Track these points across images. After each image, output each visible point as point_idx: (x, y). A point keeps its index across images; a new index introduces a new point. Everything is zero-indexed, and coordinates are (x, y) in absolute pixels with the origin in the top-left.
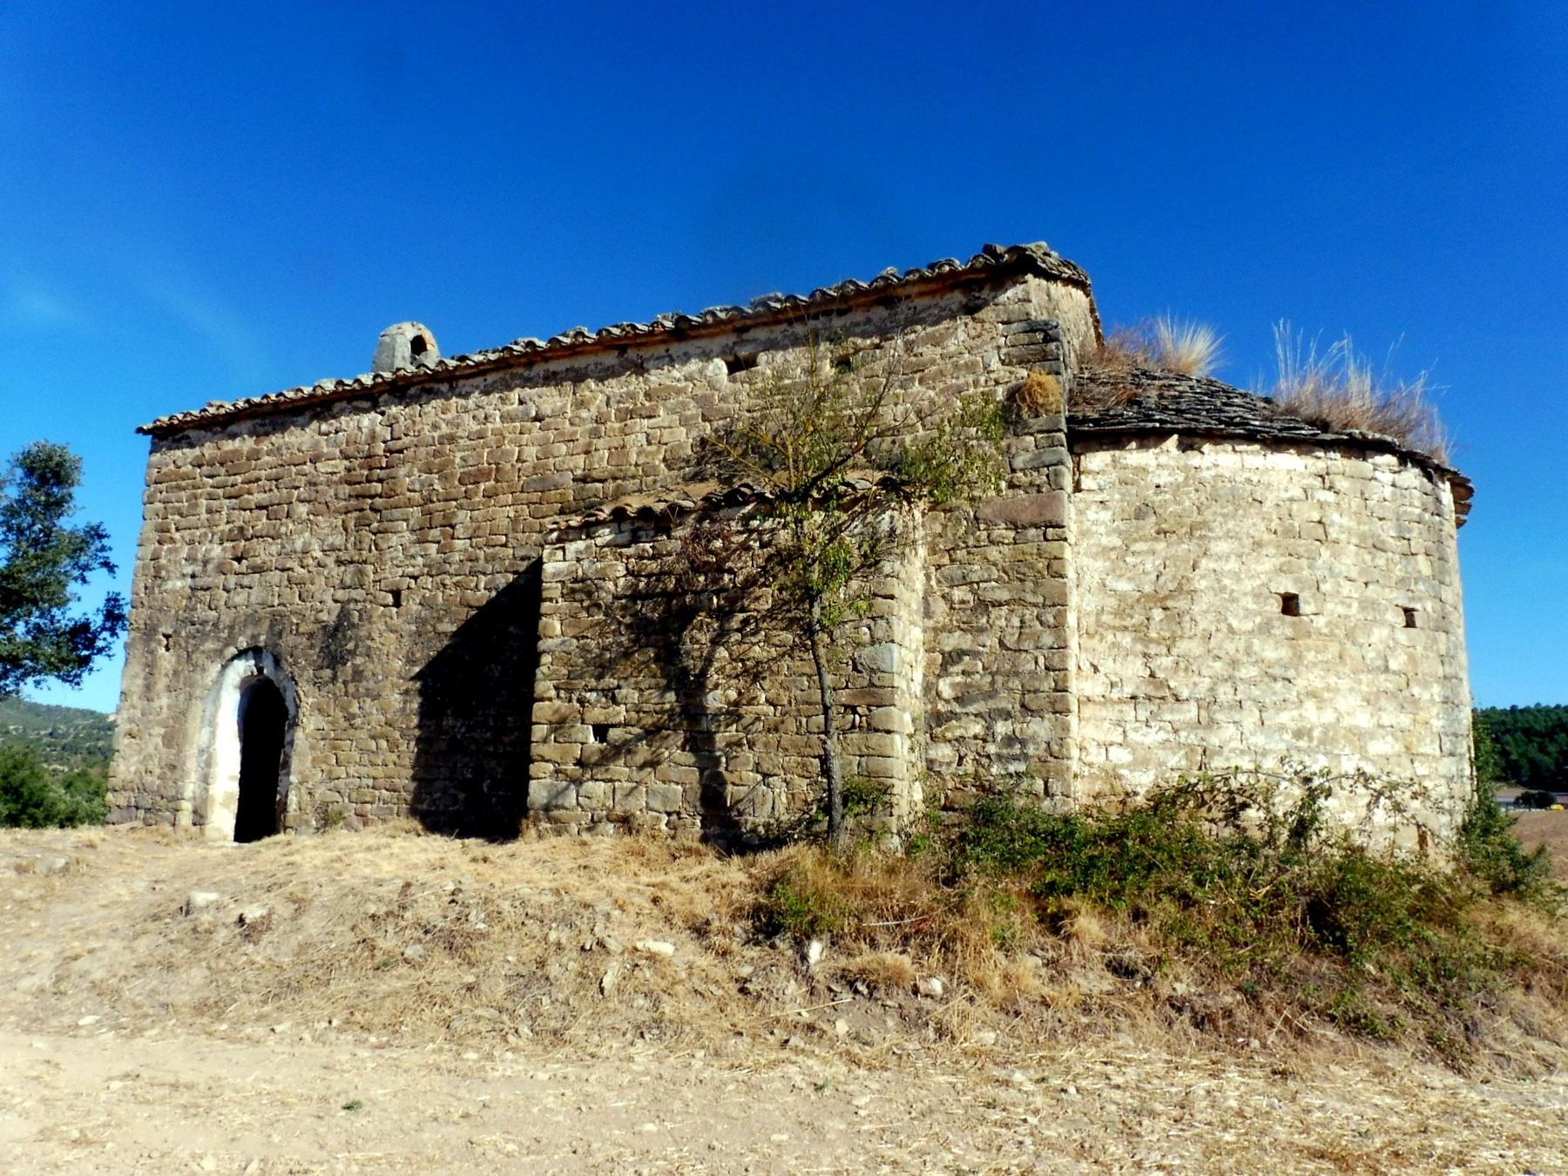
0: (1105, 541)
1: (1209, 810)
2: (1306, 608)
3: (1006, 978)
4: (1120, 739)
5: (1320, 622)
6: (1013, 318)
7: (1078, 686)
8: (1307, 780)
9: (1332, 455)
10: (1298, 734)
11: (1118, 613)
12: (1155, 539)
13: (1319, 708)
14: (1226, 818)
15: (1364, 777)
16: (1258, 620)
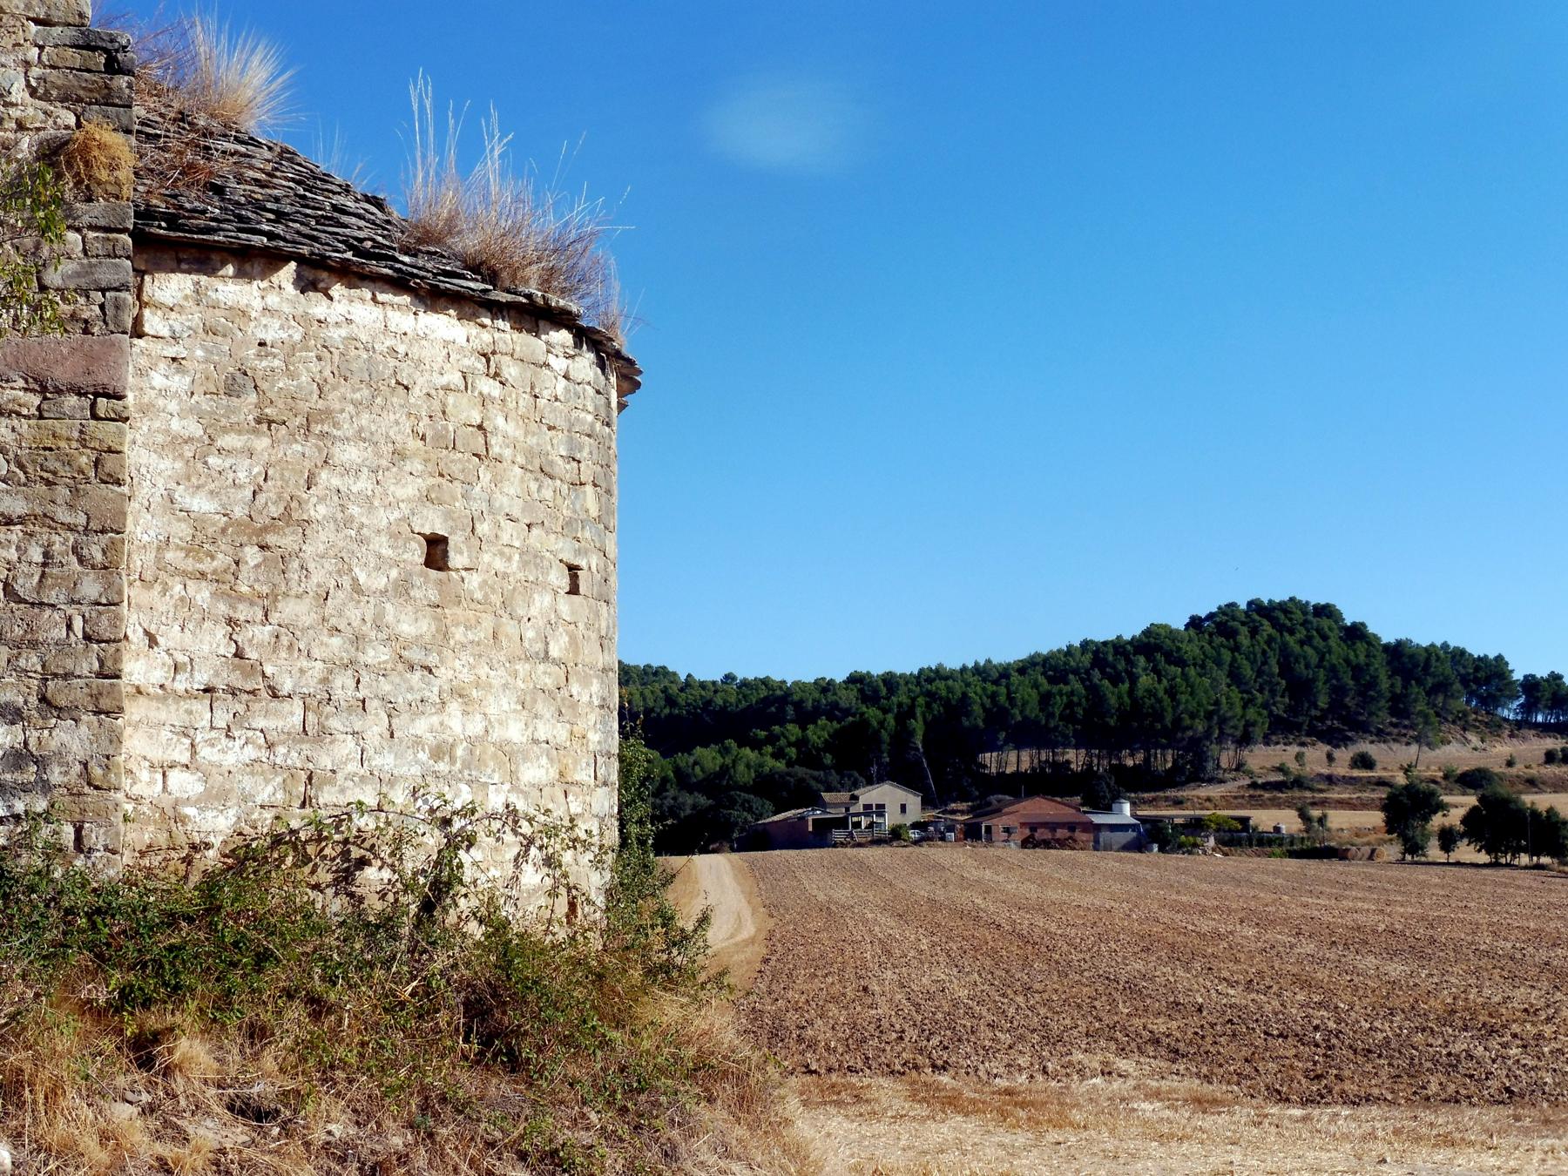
0: (175, 425)
1: (313, 872)
2: (456, 559)
3: (104, 1137)
4: (185, 758)
5: (473, 580)
6: (56, 16)
7: (138, 668)
8: (447, 822)
9: (500, 323)
10: (438, 753)
11: (193, 549)
12: (255, 431)
13: (465, 713)
14: (336, 882)
15: (512, 815)
16: (394, 573)
